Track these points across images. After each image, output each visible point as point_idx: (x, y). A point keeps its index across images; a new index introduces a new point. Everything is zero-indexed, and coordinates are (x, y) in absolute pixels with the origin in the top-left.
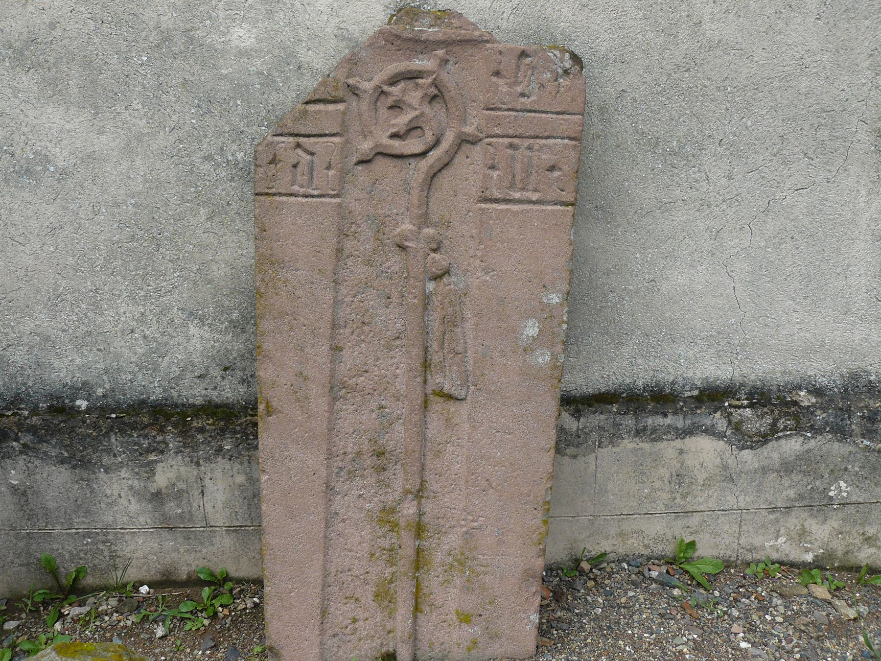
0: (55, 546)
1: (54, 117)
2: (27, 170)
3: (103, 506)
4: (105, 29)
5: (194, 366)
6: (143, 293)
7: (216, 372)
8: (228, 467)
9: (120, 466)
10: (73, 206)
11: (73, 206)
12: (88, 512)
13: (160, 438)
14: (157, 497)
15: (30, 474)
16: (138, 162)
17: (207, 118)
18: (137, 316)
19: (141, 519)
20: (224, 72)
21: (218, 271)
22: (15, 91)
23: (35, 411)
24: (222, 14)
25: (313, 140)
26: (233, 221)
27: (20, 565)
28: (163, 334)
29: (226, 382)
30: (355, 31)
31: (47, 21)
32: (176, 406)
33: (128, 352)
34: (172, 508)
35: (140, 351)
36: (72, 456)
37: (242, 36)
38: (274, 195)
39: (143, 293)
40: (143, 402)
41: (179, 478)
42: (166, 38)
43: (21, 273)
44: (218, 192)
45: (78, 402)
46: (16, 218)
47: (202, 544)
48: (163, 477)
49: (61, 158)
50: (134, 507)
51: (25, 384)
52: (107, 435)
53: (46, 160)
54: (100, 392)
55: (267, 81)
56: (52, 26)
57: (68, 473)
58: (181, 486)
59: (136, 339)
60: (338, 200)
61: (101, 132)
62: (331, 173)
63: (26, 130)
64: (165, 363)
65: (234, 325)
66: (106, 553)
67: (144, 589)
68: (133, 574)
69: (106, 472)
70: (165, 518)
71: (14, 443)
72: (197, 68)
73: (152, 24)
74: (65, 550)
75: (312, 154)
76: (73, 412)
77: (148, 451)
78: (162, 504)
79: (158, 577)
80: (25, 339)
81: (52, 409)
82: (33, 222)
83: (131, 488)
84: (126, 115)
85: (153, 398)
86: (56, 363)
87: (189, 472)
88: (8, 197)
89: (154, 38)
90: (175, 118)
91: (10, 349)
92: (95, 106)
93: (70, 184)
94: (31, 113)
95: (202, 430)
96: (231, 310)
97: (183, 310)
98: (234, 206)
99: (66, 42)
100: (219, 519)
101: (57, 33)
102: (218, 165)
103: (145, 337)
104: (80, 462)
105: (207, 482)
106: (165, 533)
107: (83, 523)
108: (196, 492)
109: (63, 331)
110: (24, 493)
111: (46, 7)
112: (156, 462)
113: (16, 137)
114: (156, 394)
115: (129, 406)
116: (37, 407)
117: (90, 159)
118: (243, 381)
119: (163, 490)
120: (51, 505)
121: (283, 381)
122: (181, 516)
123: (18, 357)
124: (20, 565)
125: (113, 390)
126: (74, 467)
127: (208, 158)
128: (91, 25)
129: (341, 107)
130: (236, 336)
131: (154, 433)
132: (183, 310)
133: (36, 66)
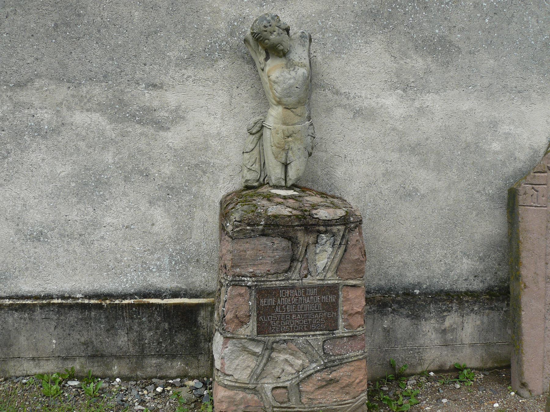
0: (396, 355)
1: (423, 174)
2: (409, 194)
3: (421, 336)
4: (446, 141)
5: (463, 275)
6: (447, 245)
7: (472, 278)
8: (475, 317)
9: (431, 318)
10: (425, 209)
11: (425, 209)
12: (414, 339)
13: (450, 305)
14: (444, 332)
15: (393, 322)
16: (452, 193)
17: (480, 176)
18: (444, 254)
19: (436, 341)
20: (488, 159)
21: (477, 237)
22: (409, 163)
23: (397, 295)
24: (489, 138)
25: (537, 186)
26: (485, 217)
27: (379, 365)
28: (453, 262)
29: (475, 282)
30: (536, 146)
31: (425, 137)
32: (455, 292)
33: (438, 269)
34: (449, 336)
35: (442, 269)
36: (413, 314)
37: (496, 146)
38: (525, 206)
39: (447, 245)
40: (442, 290)
41: (454, 323)
42: (468, 146)
43: (400, 236)
44: (481, 205)
45: (415, 291)
46: (402, 213)
47: (458, 352)
48: (447, 323)
49: (423, 190)
50: (433, 336)
51: (394, 283)
52: (429, 304)
53: (416, 190)
54: (425, 286)
55: (504, 163)
56: (427, 139)
57: (409, 321)
58: (455, 326)
59: (442, 264)
60: (545, 208)
61: (439, 181)
62: (544, 198)
63: (411, 178)
64: (452, 274)
65: (480, 258)
66: (417, 358)
67: (432, 374)
68: (425, 367)
69: (425, 321)
70: (446, 341)
71: (389, 309)
72: (479, 157)
73: (464, 140)
74: (399, 356)
75: (537, 191)
76: (414, 295)
77: (444, 311)
78: (445, 334)
79: (437, 368)
80: (397, 264)
81: (404, 294)
82: (409, 216)
83: (434, 327)
84: (450, 174)
85: (446, 289)
86: (408, 274)
87: (458, 320)
88: (400, 205)
89: (464, 145)
90: (468, 176)
91: (390, 268)
92: (439, 170)
93: (425, 200)
94: (414, 172)
95: (467, 302)
96: (480, 252)
97: (462, 252)
98: (486, 211)
99: (431, 145)
100: (467, 341)
101: (429, 142)
102: (482, 195)
103: (445, 263)
104: (415, 317)
105: (465, 324)
106: (444, 348)
107: (411, 344)
108: (460, 329)
109: (413, 261)
110: (389, 331)
111: (426, 132)
112: (447, 316)
113: (407, 181)
114: (447, 287)
115: (436, 293)
116: (398, 293)
117: (434, 191)
118: (482, 281)
119: (447, 328)
120: (399, 336)
121: (530, 275)
122: (452, 340)
123: (393, 271)
124: (379, 365)
125: (430, 286)
126: (412, 319)
127: (479, 192)
128: (441, 139)
129: (546, 174)
130: (481, 263)
131: (448, 303)
132: (462, 252)
133: (419, 154)
